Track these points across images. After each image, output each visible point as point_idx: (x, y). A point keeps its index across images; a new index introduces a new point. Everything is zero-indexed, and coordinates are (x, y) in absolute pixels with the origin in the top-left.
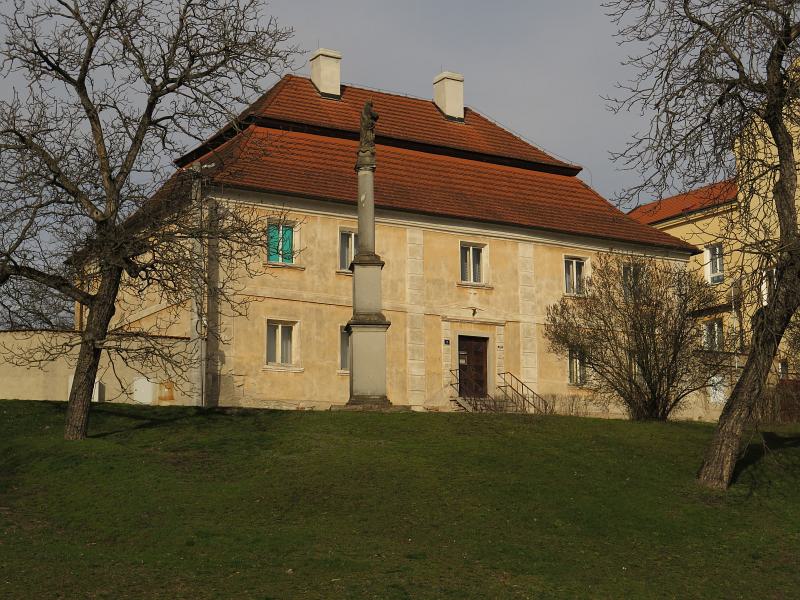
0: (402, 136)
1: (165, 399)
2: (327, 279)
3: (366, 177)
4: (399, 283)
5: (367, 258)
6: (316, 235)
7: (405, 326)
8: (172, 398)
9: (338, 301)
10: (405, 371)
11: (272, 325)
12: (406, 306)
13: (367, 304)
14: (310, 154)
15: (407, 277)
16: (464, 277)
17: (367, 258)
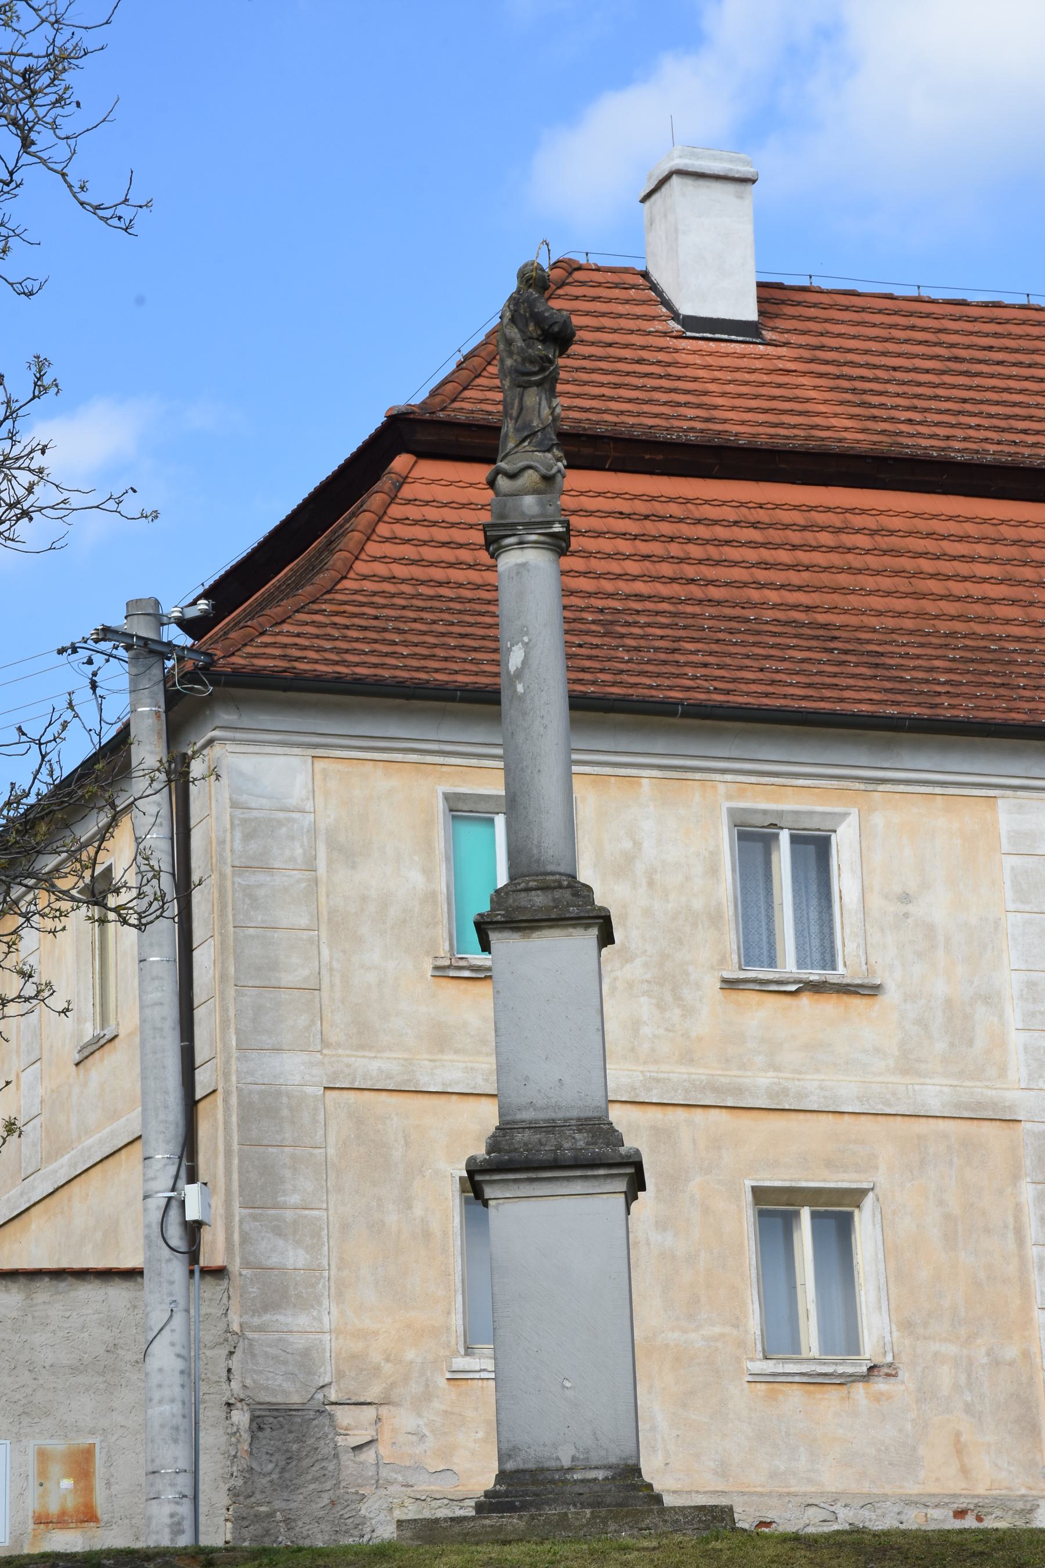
0: (992, 452)
1: (61, 1521)
2: (689, 1012)
3: (530, 581)
4: (981, 1011)
5: (539, 899)
6: (637, 844)
7: (1015, 1178)
8: (88, 1516)
9: (739, 1090)
10: (1026, 1355)
11: (775, 1209)
12: (1012, 1096)
13: (556, 1087)
14: (625, 546)
15: (1010, 982)
16: (758, 944)
17: (539, 899)
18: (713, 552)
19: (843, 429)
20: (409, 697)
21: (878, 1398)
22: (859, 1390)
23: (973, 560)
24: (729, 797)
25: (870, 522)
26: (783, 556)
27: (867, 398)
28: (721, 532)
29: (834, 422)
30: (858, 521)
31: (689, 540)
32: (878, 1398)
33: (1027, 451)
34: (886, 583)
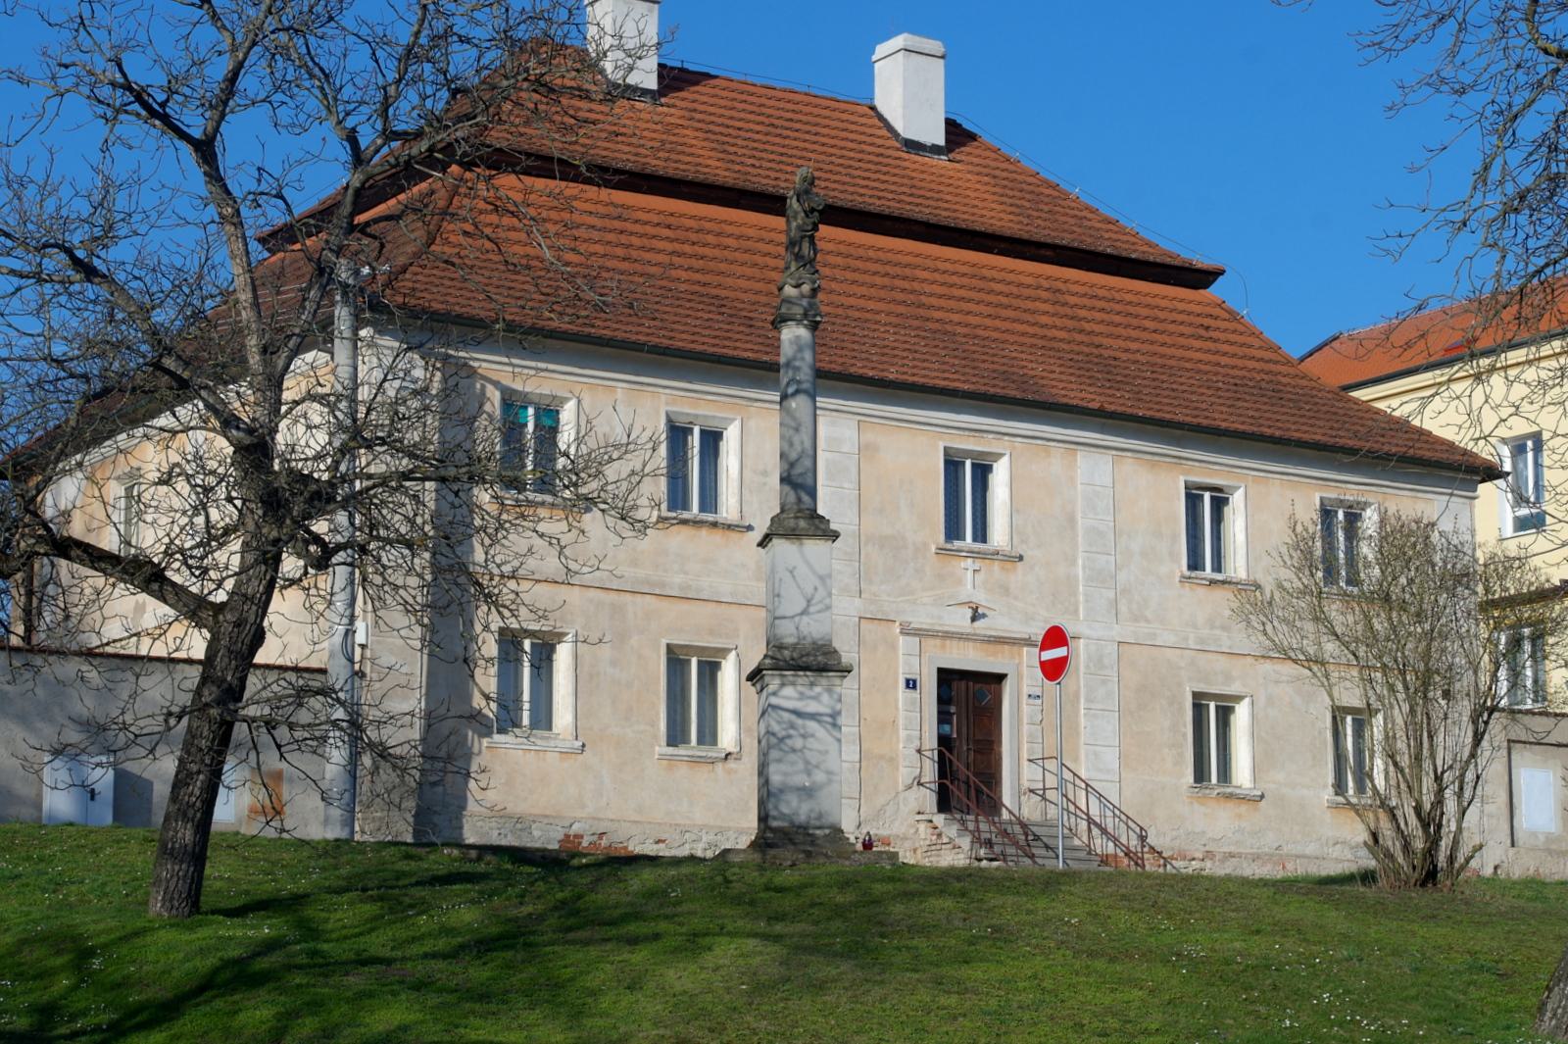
9: (663, 585)
18: (646, 242)
19: (719, 172)
20: (1049, 409)
21: (729, 772)
22: (719, 766)
23: (1036, 300)
24: (667, 404)
25: (736, 231)
26: (687, 248)
27: (726, 147)
28: (649, 229)
29: (709, 162)
30: (730, 229)
31: (632, 234)
32: (729, 772)
33: (908, 207)
34: (748, 271)
